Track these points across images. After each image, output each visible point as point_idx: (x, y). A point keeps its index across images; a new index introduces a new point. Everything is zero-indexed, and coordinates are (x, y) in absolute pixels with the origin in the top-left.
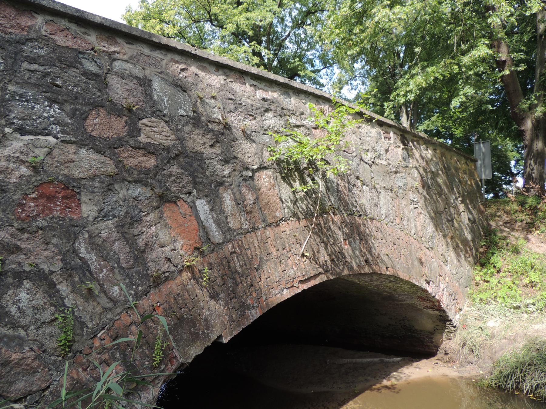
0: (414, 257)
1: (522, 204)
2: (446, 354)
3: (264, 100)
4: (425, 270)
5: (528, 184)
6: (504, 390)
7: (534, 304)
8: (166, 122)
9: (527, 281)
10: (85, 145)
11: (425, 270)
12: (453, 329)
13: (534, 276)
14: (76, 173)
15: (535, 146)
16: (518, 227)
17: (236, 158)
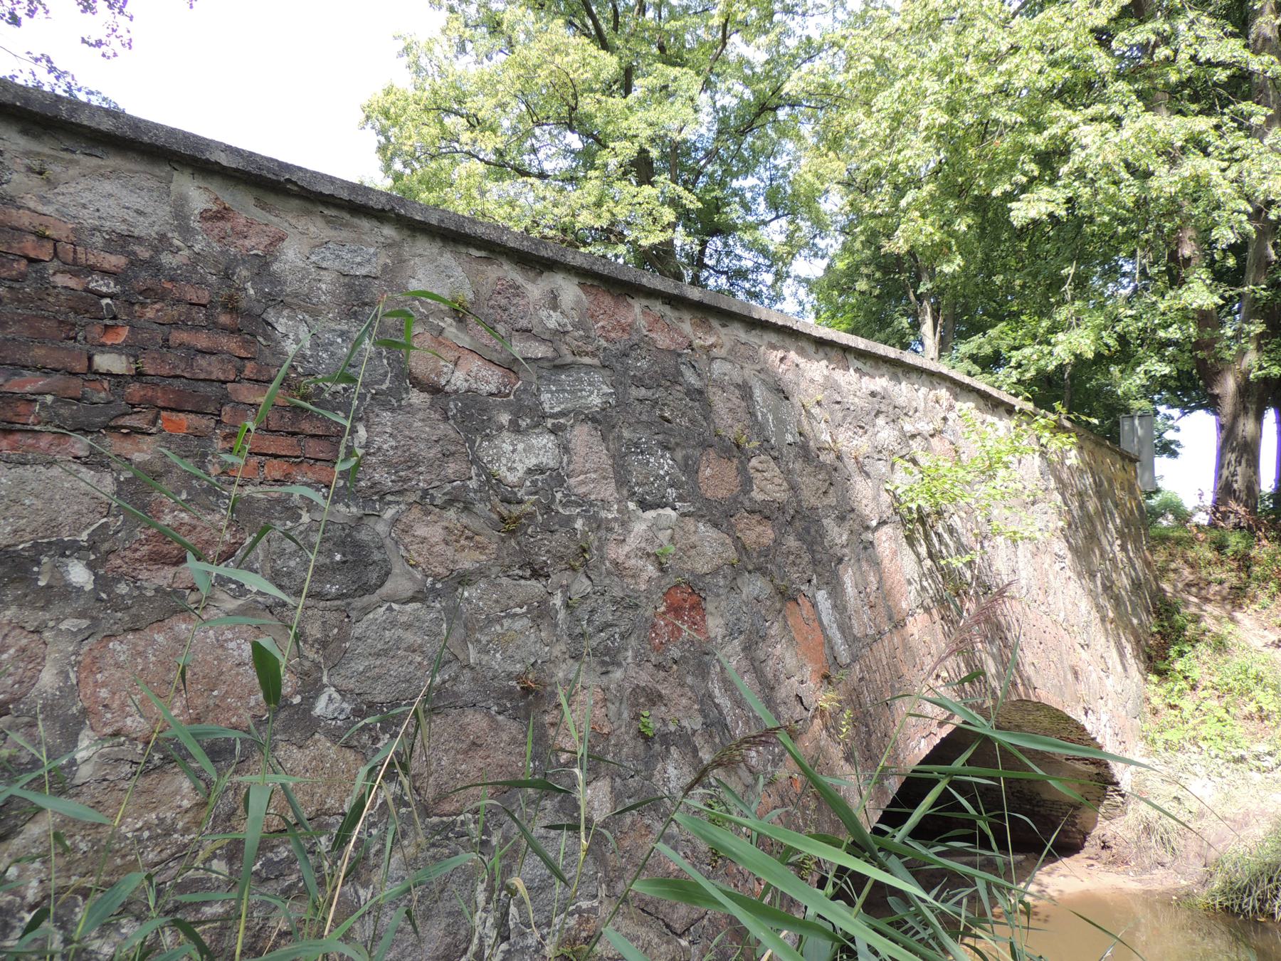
0: (1066, 664)
1: (1220, 547)
2: (1105, 847)
3: (873, 394)
4: (1082, 688)
5: (1226, 504)
6: (1238, 915)
7: (1270, 754)
8: (775, 458)
9: (1252, 707)
10: (703, 516)
11: (1082, 688)
12: (1119, 799)
13: (1267, 700)
14: (702, 567)
15: (1241, 427)
16: (1214, 595)
17: (853, 510)
